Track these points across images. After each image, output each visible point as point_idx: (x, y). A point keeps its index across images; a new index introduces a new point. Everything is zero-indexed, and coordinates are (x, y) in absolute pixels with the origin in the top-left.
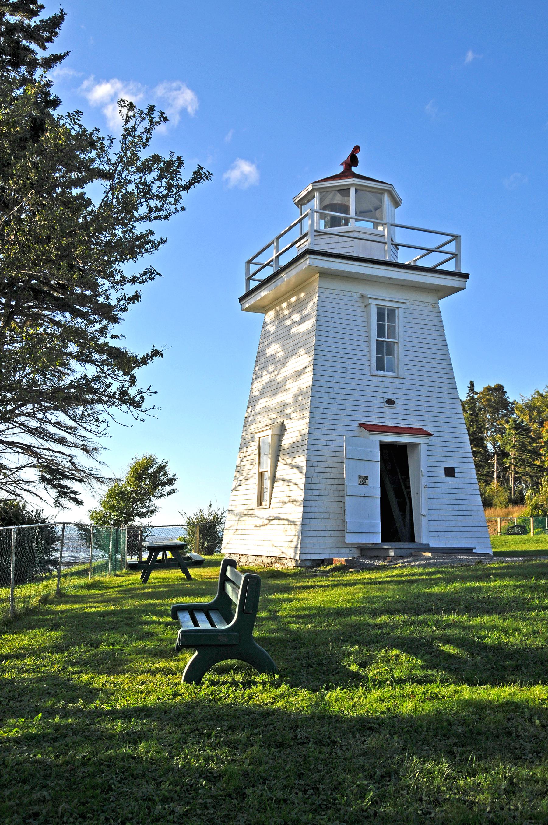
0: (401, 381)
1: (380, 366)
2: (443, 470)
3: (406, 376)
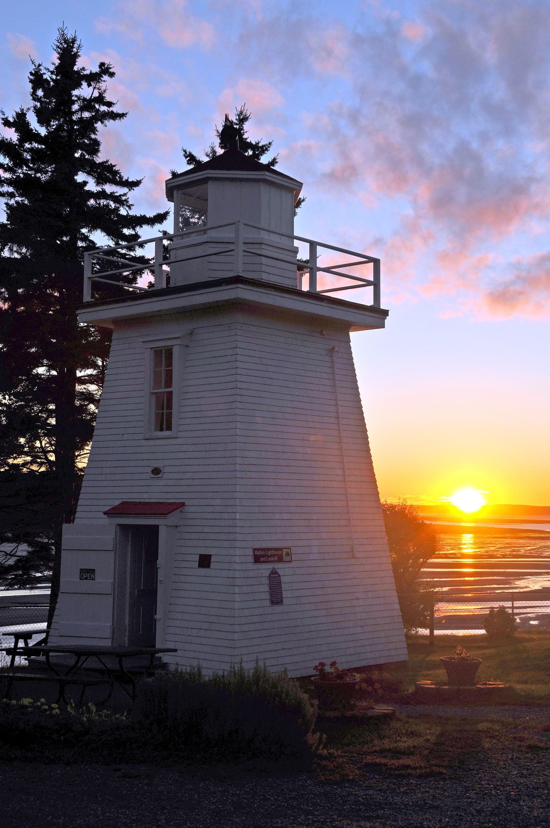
3: (180, 434)
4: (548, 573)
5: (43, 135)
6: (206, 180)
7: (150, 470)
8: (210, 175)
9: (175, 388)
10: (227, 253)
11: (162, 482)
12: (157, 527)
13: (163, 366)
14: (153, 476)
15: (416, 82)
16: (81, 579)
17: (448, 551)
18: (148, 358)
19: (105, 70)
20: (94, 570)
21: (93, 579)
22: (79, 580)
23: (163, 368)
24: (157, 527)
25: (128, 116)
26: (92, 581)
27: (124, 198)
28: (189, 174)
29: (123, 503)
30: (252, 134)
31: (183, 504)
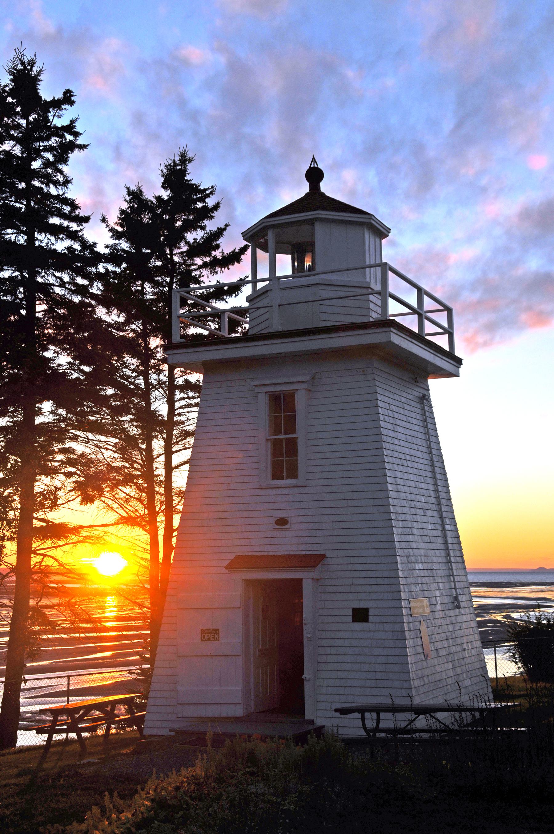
0: (302, 490)
1: (277, 475)
2: (371, 619)
4: (1, 644)
5: (33, 163)
6: (311, 222)
7: (273, 521)
8: (319, 216)
9: (300, 434)
10: (352, 298)
11: (289, 534)
12: (299, 582)
13: (282, 412)
14: (277, 527)
15: (193, 116)
16: (202, 640)
17: (100, 614)
18: (263, 402)
19: (68, 98)
20: (218, 630)
21: (217, 640)
22: (200, 641)
23: (282, 414)
24: (299, 582)
25: (89, 148)
26: (217, 641)
27: (80, 234)
28: (282, 215)
29: (238, 557)
30: (196, 175)
31: (323, 556)
